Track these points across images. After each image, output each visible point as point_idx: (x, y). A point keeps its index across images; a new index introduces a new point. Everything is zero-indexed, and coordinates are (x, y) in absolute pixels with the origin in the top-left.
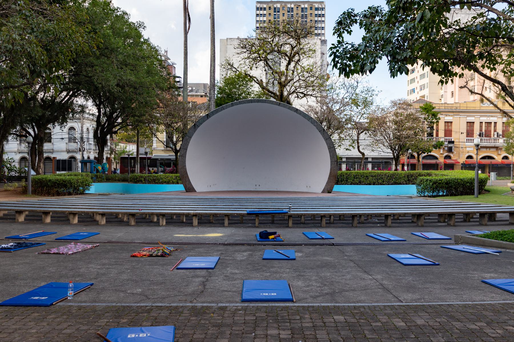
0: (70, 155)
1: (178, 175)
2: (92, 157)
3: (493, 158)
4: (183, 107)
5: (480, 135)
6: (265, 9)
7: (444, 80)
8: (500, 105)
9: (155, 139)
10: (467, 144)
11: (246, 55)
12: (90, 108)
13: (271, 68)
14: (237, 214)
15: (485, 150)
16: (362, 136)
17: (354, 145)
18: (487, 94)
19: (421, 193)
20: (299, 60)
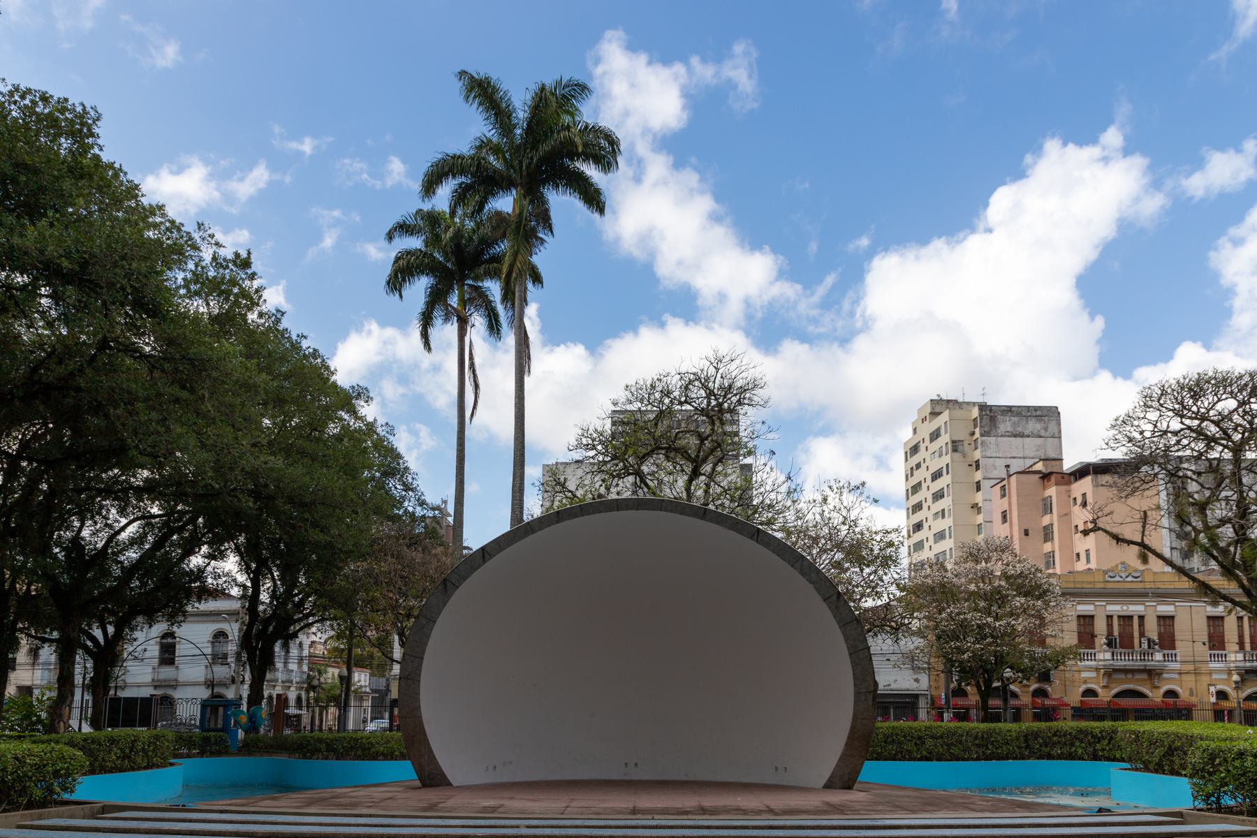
15: (1122, 676)
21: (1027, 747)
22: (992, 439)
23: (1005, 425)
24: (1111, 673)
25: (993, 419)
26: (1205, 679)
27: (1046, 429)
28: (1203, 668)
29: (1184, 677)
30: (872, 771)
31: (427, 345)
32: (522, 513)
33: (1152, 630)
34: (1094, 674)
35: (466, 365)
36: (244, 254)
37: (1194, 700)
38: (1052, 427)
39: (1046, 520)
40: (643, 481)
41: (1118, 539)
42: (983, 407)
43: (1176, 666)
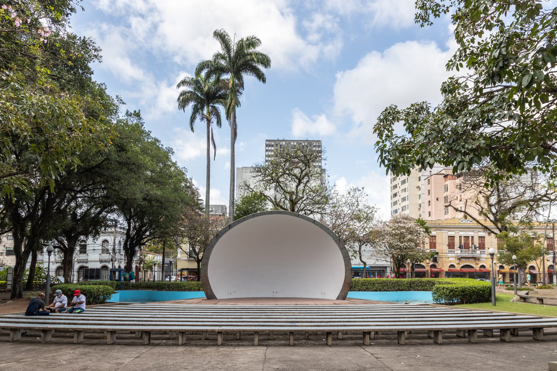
0: (103, 264)
1: (200, 282)
3: (473, 267)
4: (206, 223)
5: (460, 247)
6: (273, 146)
7: (489, 183)
8: (482, 222)
9: (179, 250)
10: (449, 255)
11: (261, 178)
12: (121, 222)
13: (282, 189)
14: (269, 330)
16: (363, 247)
17: (355, 255)
20: (308, 181)
24: (460, 259)
30: (351, 294)
31: (192, 129)
33: (477, 242)
34: (454, 259)
35: (210, 138)
36: (137, 111)
41: (457, 210)
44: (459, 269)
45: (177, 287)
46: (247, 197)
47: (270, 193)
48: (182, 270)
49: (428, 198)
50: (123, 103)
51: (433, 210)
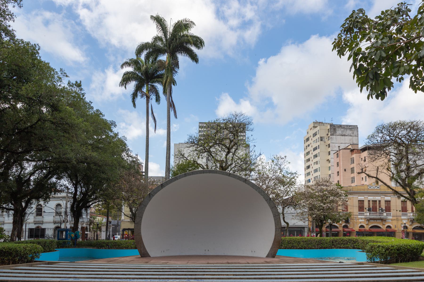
2: (68, 227)
3: (379, 227)
5: (369, 210)
11: (194, 148)
13: (213, 157)
15: (373, 221)
18: (380, 176)
19: (371, 260)
21: (333, 245)
22: (334, 137)
23: (339, 131)
24: (369, 220)
25: (335, 129)
26: (400, 222)
27: (353, 133)
28: (399, 218)
29: (393, 221)
30: (281, 252)
31: (134, 105)
32: (169, 166)
33: (383, 206)
36: (79, 82)
37: (396, 229)
38: (355, 132)
39: (352, 166)
40: (210, 154)
41: (369, 176)
42: (331, 125)
43: (391, 217)
44: (368, 229)
45: (117, 246)
46: (181, 165)
47: (202, 161)
48: (124, 230)
49: (337, 169)
50: (67, 76)
51: (342, 179)
